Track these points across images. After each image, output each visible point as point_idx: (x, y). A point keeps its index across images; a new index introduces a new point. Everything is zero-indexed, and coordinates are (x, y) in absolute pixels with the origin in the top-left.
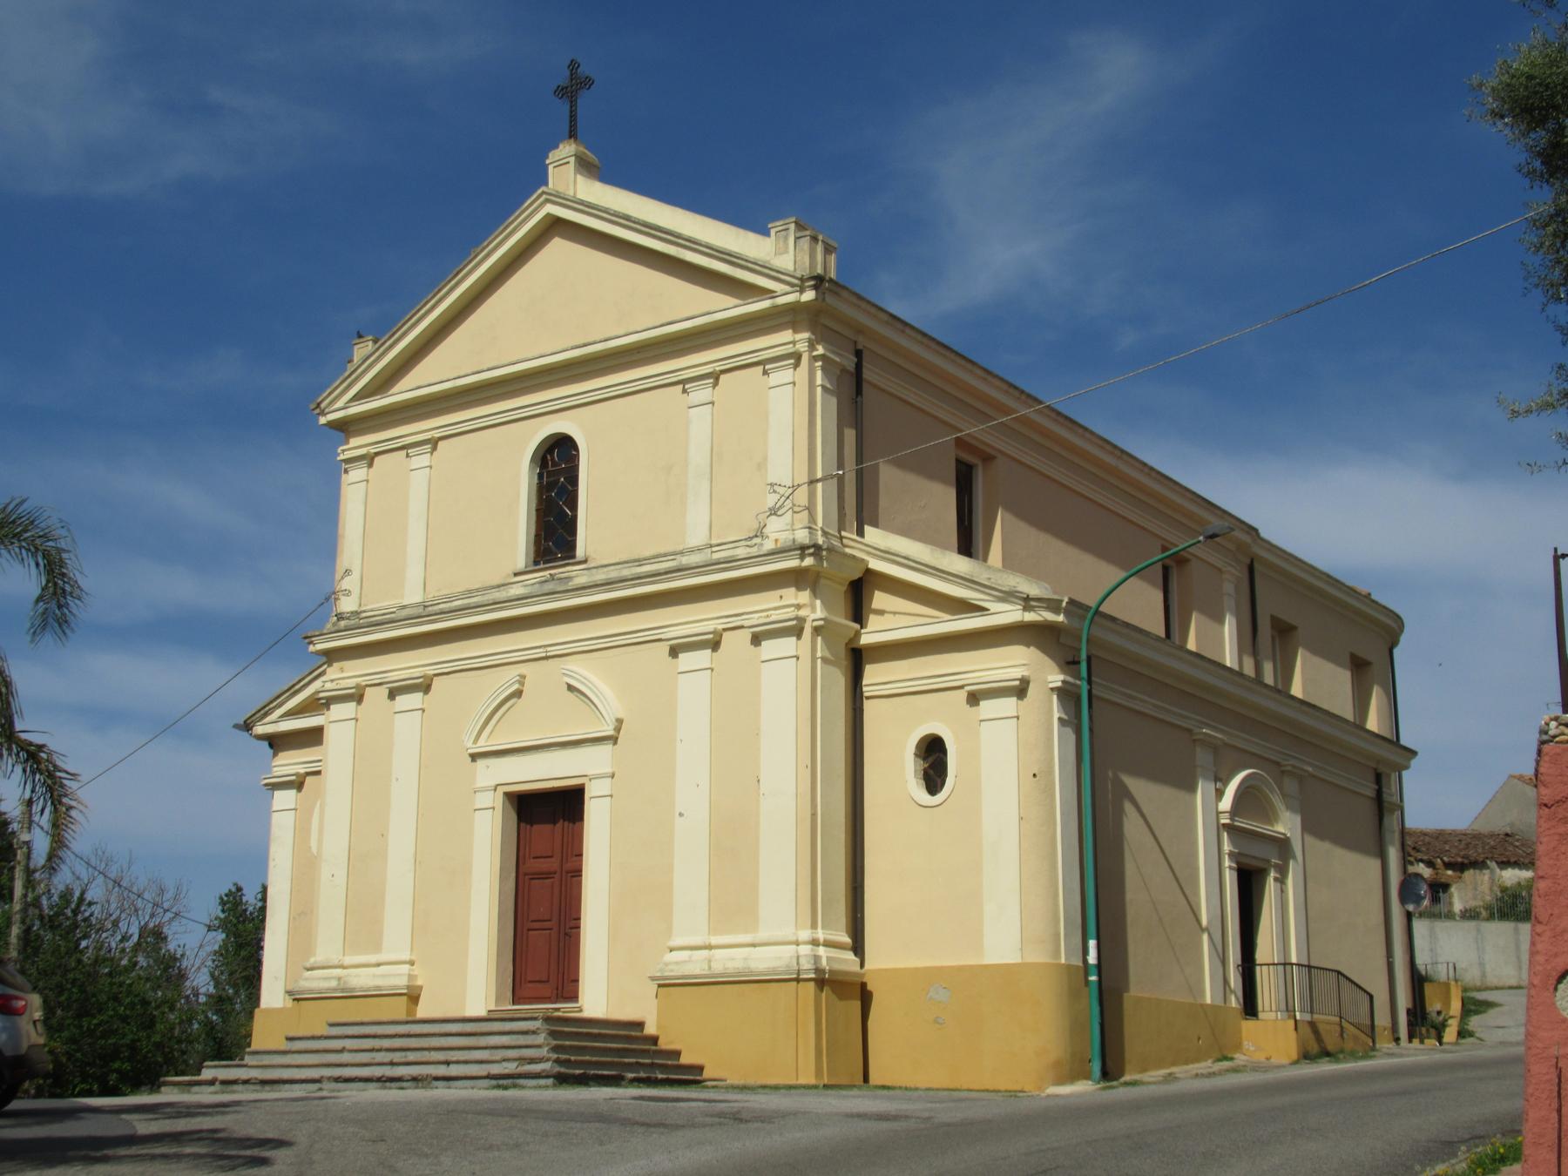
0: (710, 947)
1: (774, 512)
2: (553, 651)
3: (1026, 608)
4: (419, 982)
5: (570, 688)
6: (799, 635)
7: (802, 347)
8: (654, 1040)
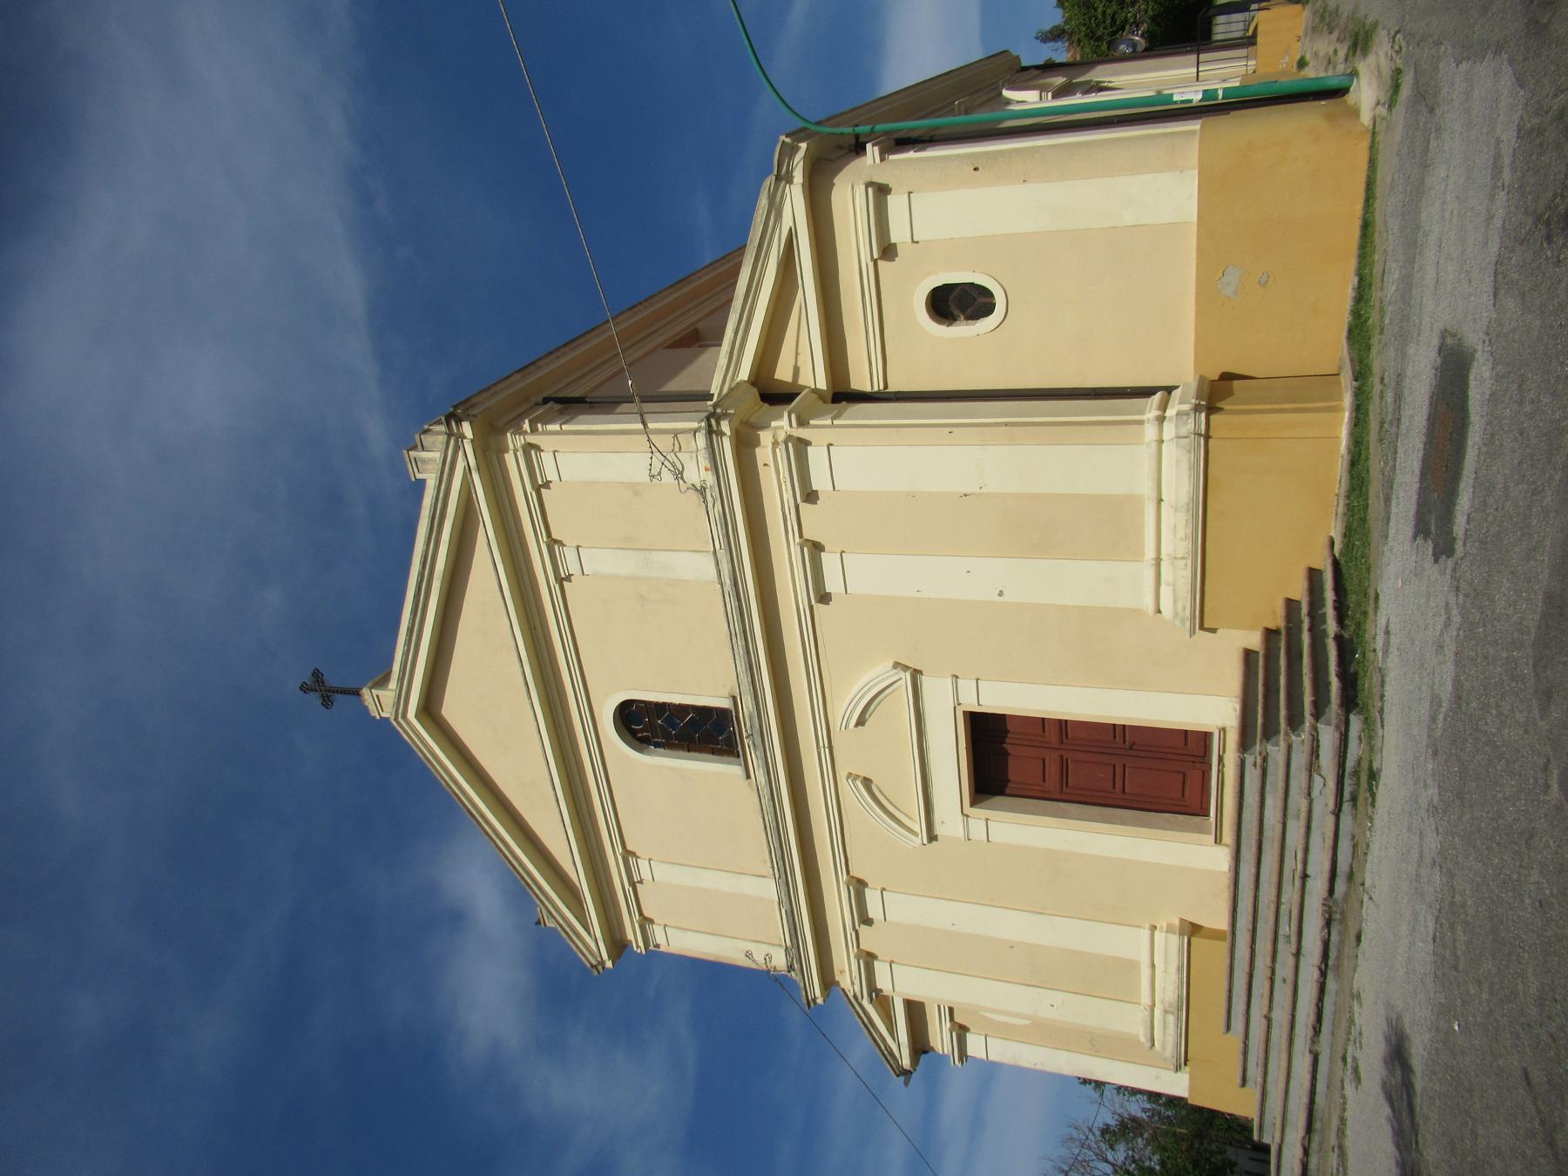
1: (679, 475)
2: (824, 741)
3: (790, 180)
4: (1177, 922)
5: (861, 722)
6: (807, 443)
7: (520, 441)
8: (1270, 634)
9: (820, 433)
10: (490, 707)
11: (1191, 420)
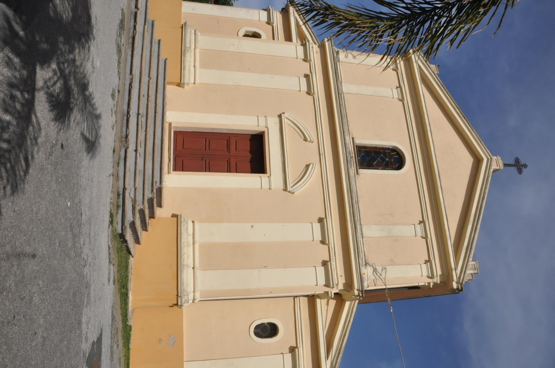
0: (194, 243)
1: (375, 270)
4: (186, 87)
5: (308, 166)
6: (325, 286)
7: (435, 280)
8: (152, 216)
9: (321, 290)
10: (453, 161)
11: (183, 301)
